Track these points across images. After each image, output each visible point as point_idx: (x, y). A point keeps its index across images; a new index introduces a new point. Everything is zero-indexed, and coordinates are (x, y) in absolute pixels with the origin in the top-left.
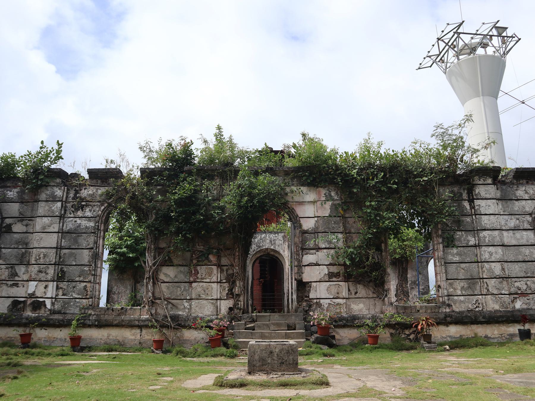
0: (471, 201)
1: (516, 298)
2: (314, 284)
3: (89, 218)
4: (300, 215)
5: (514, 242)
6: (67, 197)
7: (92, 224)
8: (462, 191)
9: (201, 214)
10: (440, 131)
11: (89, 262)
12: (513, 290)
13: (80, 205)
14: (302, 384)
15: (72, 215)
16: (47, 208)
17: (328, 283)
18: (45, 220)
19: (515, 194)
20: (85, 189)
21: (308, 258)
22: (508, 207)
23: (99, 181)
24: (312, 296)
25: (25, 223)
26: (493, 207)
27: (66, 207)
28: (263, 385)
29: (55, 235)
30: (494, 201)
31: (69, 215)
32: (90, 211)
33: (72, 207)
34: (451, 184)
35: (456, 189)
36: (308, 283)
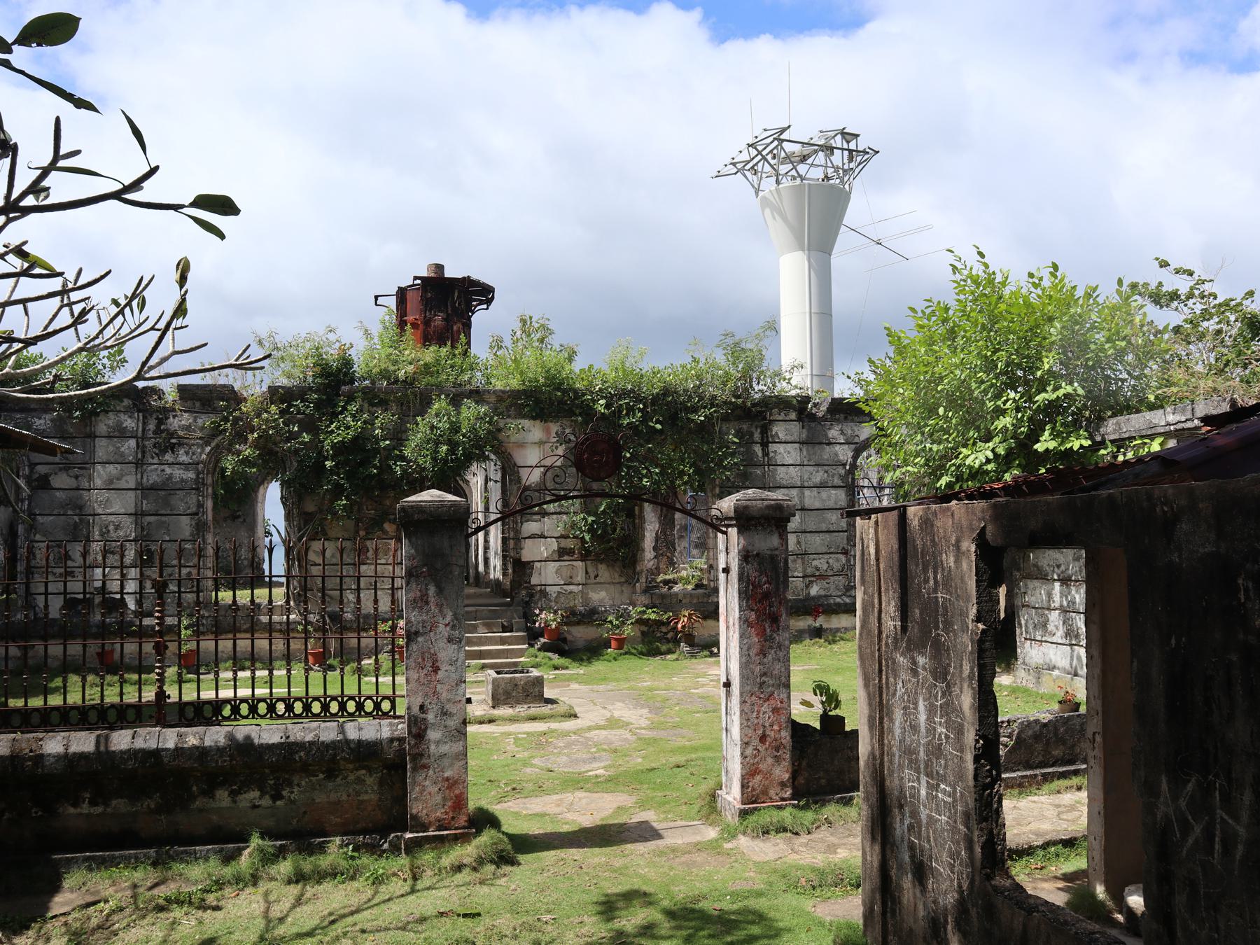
0: (765, 445)
1: (811, 582)
2: (537, 565)
3: (186, 466)
4: (520, 463)
5: (817, 505)
6: (144, 430)
7: (191, 475)
8: (753, 430)
9: (375, 467)
10: (730, 341)
11: (192, 535)
12: (809, 571)
13: (169, 443)
14: (552, 717)
15: (156, 461)
16: (111, 448)
17: (558, 564)
18: (110, 468)
19: (826, 435)
20: (174, 417)
21: (531, 527)
22: (815, 454)
23: (198, 404)
24: (534, 581)
25: (71, 472)
26: (793, 454)
27: (144, 446)
28: (513, 720)
29: (131, 494)
30: (797, 445)
31: (151, 461)
32: (187, 453)
33: (155, 446)
34: (739, 419)
35: (745, 427)
36: (529, 563)
